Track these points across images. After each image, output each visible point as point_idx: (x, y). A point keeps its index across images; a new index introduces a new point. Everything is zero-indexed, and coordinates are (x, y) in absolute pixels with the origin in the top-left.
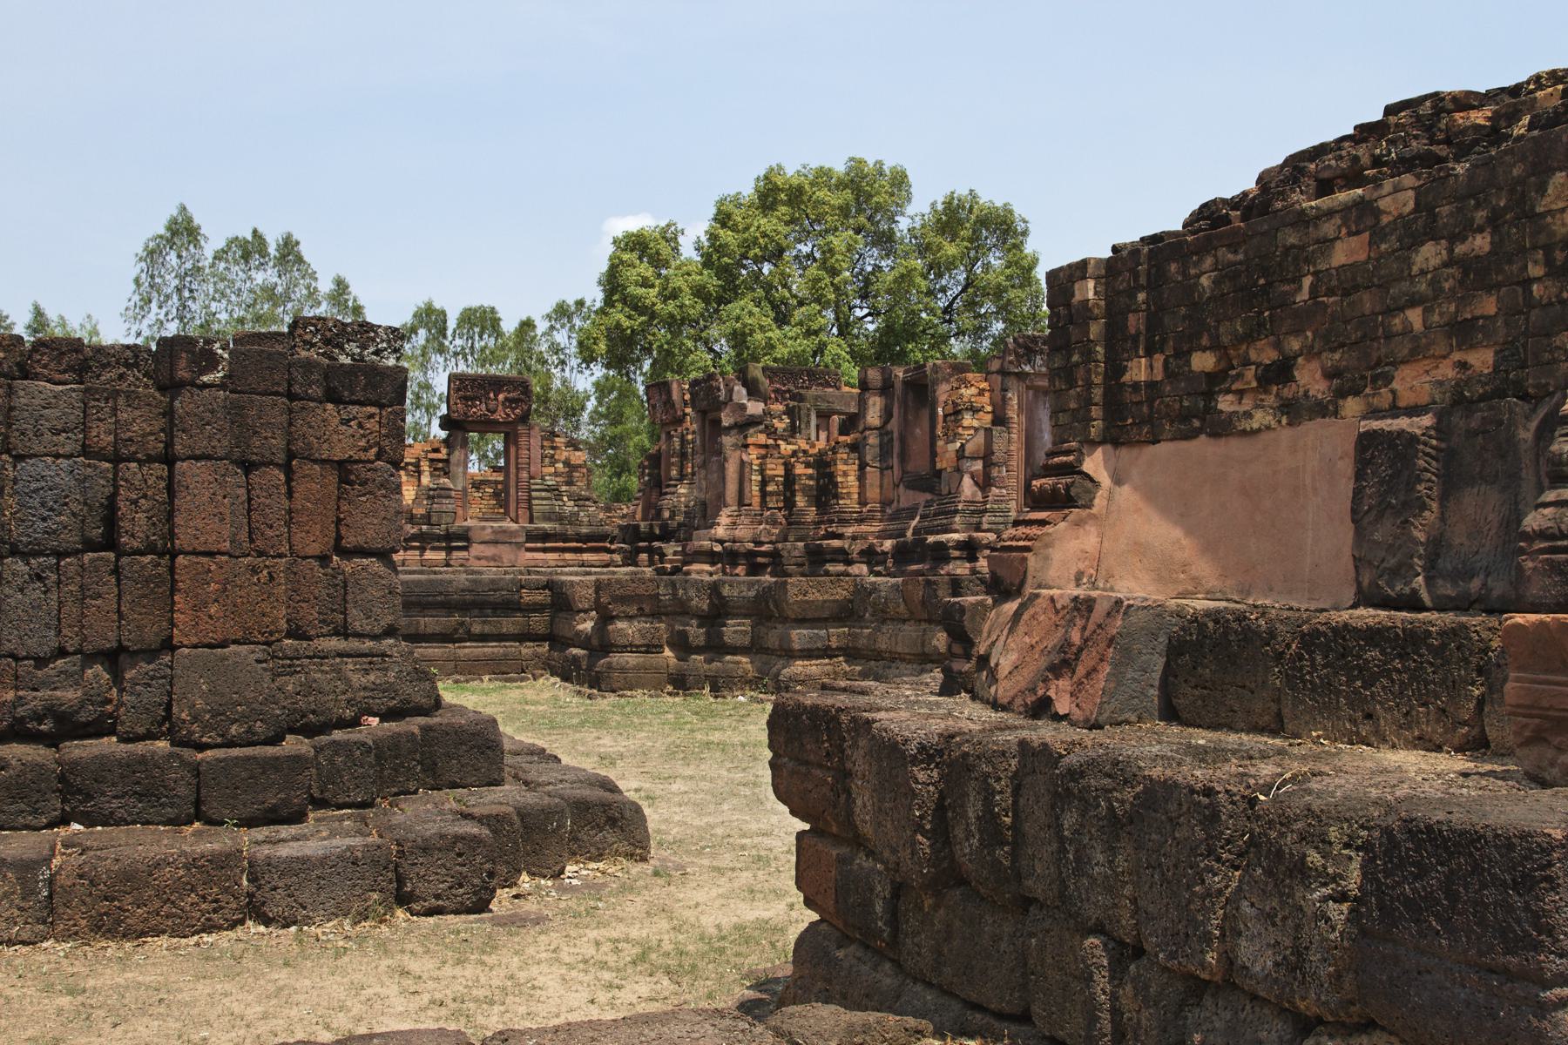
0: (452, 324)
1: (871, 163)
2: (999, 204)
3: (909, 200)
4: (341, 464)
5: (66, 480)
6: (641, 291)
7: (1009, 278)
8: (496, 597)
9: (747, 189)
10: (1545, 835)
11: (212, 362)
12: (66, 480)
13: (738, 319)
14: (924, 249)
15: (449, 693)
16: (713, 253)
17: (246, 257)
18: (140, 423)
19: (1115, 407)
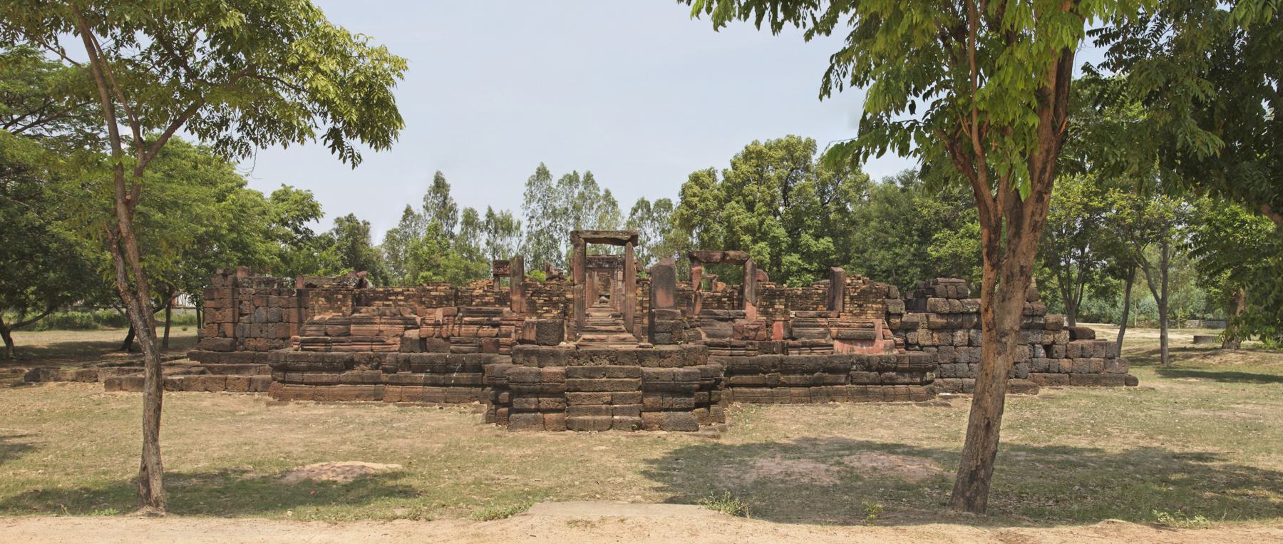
0: (652, 207)
3: (815, 153)
10: (1096, 450)
17: (571, 182)
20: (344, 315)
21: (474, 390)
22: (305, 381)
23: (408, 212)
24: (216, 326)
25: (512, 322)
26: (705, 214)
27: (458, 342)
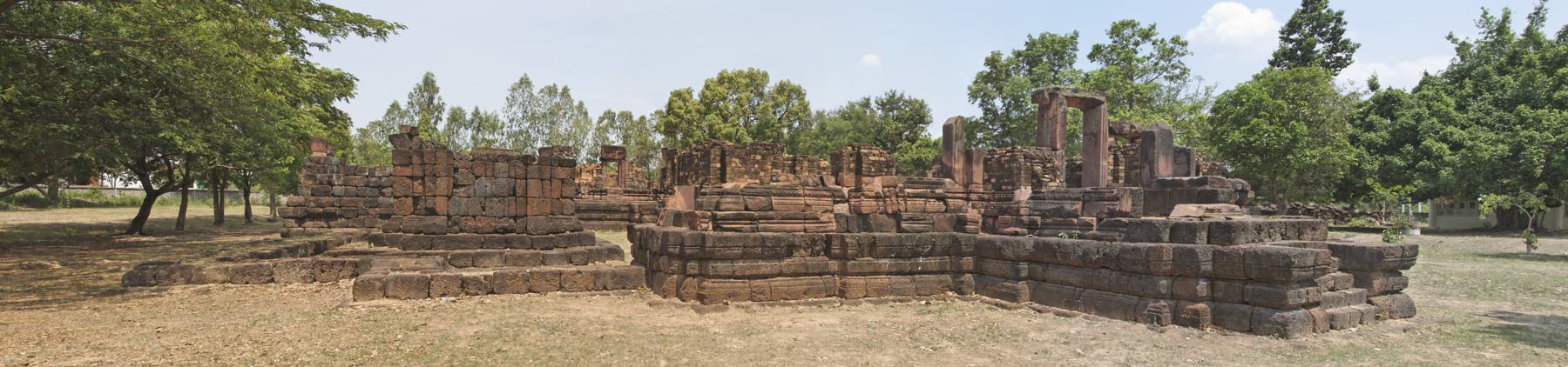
1: (756, 69)
3: (768, 82)
4: (562, 180)
5: (505, 183)
6: (678, 110)
7: (800, 109)
8: (613, 208)
9: (715, 76)
11: (535, 160)
12: (505, 183)
14: (773, 99)
15: (598, 235)
16: (703, 96)
18: (520, 172)
19: (679, 179)
20: (762, 183)
21: (942, 277)
22: (738, 274)
23: (395, 106)
24: (410, 201)
25: (957, 195)
26: (690, 122)
27: (911, 219)
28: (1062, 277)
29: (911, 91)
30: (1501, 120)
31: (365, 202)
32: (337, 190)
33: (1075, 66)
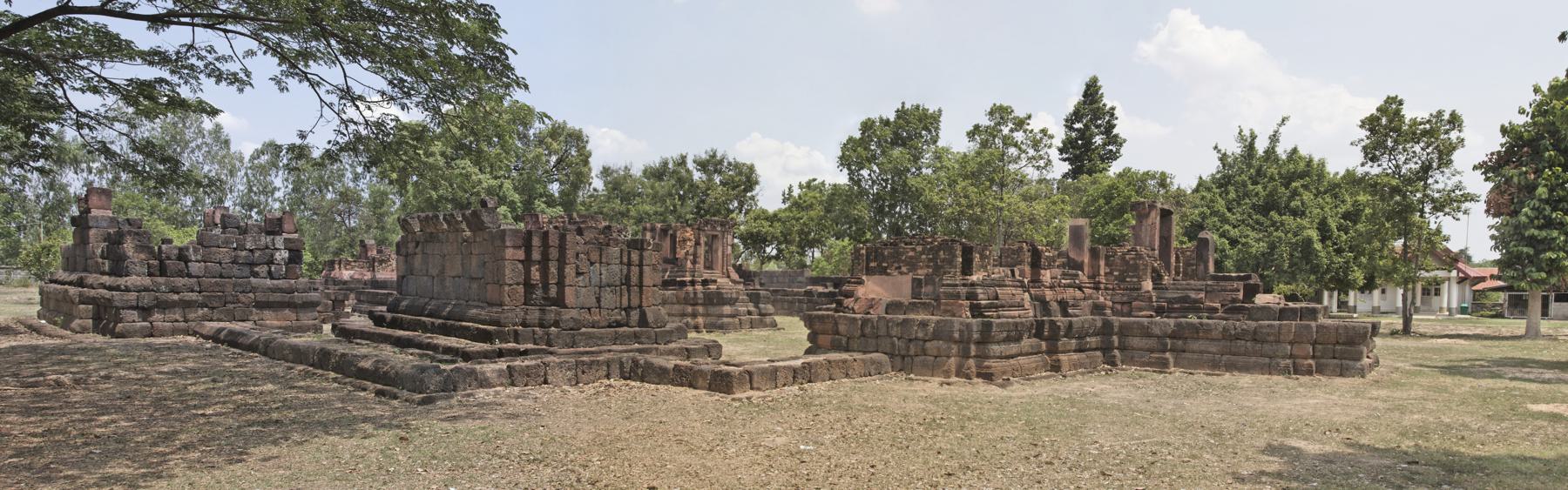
2: (577, 128)
13: (463, 168)
28: (1202, 348)
29: (739, 151)
30: (1257, 222)
31: (235, 285)
32: (195, 267)
33: (938, 144)
